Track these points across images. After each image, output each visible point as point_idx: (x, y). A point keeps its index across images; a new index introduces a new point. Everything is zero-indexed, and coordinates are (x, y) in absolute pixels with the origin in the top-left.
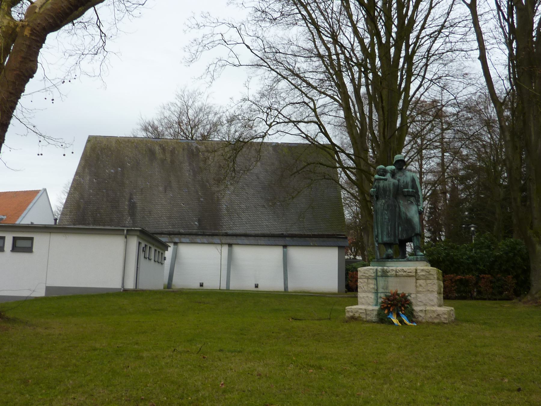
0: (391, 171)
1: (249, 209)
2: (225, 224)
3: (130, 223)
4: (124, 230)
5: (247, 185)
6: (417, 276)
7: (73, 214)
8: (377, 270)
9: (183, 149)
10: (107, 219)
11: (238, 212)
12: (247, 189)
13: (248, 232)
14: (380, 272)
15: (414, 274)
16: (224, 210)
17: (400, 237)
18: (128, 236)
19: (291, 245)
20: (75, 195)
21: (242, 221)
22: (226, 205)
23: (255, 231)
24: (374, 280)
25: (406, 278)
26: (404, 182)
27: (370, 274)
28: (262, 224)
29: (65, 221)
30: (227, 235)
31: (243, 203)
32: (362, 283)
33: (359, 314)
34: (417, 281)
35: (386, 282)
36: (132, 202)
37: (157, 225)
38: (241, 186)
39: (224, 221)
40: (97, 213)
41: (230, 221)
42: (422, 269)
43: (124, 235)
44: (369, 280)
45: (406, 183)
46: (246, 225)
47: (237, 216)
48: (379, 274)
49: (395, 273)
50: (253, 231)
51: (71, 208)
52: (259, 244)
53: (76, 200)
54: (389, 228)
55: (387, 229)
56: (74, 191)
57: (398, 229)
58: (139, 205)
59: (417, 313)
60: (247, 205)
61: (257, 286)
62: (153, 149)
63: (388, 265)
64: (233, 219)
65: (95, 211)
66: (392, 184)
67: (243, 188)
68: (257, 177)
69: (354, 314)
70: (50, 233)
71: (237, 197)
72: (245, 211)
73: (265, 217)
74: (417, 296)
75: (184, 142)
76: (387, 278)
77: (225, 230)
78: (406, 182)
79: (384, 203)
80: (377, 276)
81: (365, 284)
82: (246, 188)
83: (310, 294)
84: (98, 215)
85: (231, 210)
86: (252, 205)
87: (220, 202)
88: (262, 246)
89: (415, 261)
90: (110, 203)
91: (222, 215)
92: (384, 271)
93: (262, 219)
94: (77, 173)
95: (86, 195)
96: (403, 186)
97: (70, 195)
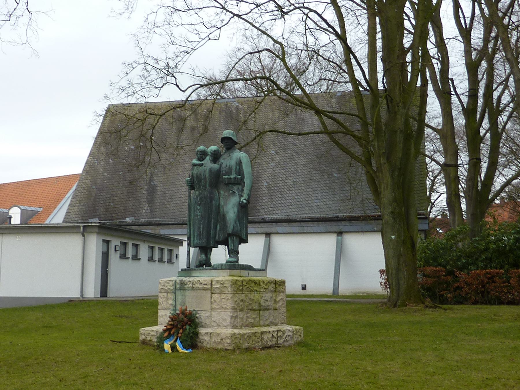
0: (211, 153)
1: (297, 186)
2: (263, 207)
3: (147, 211)
4: (79, 227)
5: (297, 153)
6: (212, 289)
7: (82, 204)
8: (176, 281)
9: (220, 112)
10: (121, 208)
11: (282, 190)
12: (297, 159)
13: (293, 217)
14: (178, 284)
15: (209, 287)
16: (265, 189)
17: (217, 238)
18: (85, 234)
19: (347, 231)
20: (87, 181)
21: (285, 202)
22: (267, 182)
23: (301, 214)
24: (173, 294)
25: (202, 291)
26: (226, 166)
27: (169, 287)
28: (312, 205)
29: (72, 213)
30: (264, 221)
31: (290, 178)
32: (161, 298)
33: (151, 337)
34: (213, 295)
35: (184, 297)
36: (152, 185)
37: (178, 213)
38: (289, 155)
39: (263, 204)
40: (110, 201)
41: (270, 203)
42: (218, 281)
43: (80, 232)
44: (169, 294)
45: (229, 167)
46: (291, 207)
47: (280, 196)
48: (178, 286)
49: (191, 285)
50: (299, 214)
51: (81, 197)
52: (305, 232)
53: (87, 187)
54: (202, 227)
55: (199, 228)
56: (85, 176)
57: (216, 228)
58: (159, 188)
59: (202, 336)
60: (295, 180)
61: (304, 288)
62: (183, 115)
63: (194, 275)
64: (274, 200)
65: (108, 199)
66: (208, 169)
67: (292, 157)
68: (312, 141)
69: (146, 337)
70: (2, 233)
71: (282, 171)
72: (291, 189)
73: (317, 195)
74: (211, 314)
75: (222, 102)
76: (184, 291)
77: (263, 215)
78: (230, 165)
79: (197, 196)
80: (176, 289)
81: (164, 299)
82: (296, 157)
83: (326, 299)
84: (112, 204)
85: (273, 188)
86: (301, 180)
87: (260, 179)
88: (310, 234)
89: (220, 269)
90: (127, 189)
91: (261, 195)
92: (182, 283)
93: (313, 198)
94: (91, 154)
95: (99, 180)
96: (225, 171)
97: (81, 182)
